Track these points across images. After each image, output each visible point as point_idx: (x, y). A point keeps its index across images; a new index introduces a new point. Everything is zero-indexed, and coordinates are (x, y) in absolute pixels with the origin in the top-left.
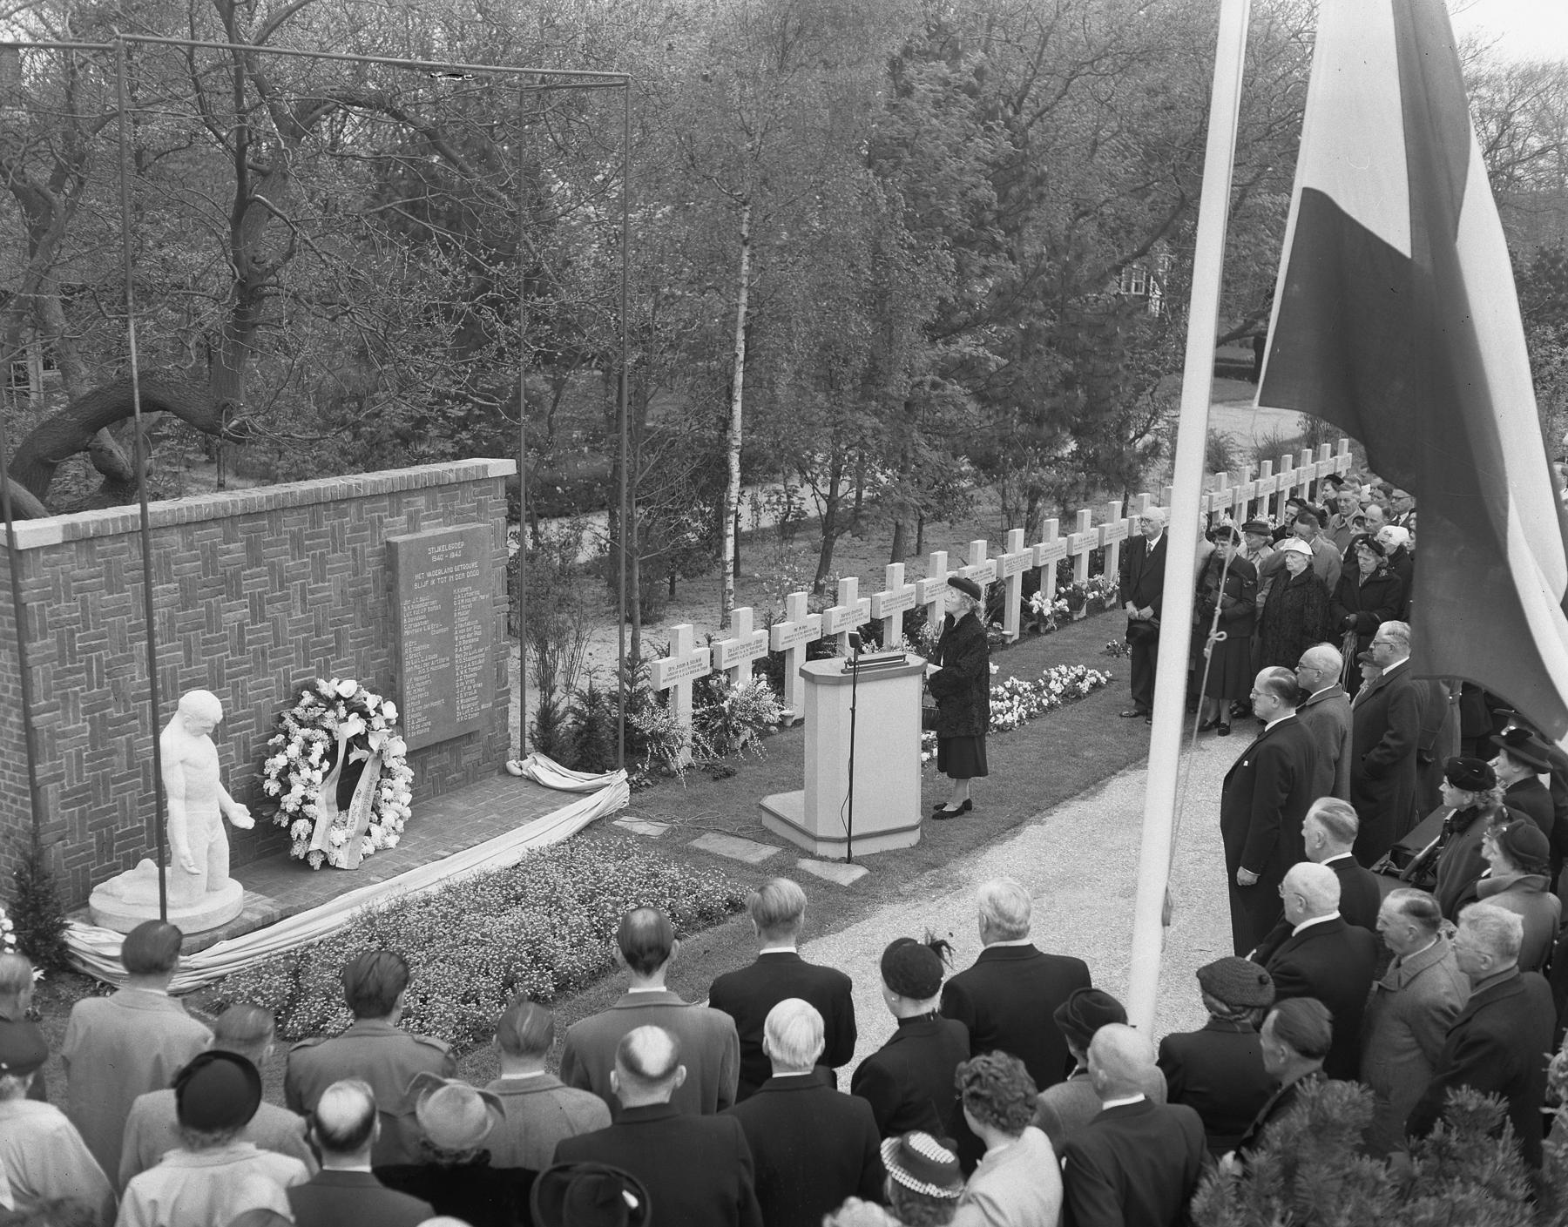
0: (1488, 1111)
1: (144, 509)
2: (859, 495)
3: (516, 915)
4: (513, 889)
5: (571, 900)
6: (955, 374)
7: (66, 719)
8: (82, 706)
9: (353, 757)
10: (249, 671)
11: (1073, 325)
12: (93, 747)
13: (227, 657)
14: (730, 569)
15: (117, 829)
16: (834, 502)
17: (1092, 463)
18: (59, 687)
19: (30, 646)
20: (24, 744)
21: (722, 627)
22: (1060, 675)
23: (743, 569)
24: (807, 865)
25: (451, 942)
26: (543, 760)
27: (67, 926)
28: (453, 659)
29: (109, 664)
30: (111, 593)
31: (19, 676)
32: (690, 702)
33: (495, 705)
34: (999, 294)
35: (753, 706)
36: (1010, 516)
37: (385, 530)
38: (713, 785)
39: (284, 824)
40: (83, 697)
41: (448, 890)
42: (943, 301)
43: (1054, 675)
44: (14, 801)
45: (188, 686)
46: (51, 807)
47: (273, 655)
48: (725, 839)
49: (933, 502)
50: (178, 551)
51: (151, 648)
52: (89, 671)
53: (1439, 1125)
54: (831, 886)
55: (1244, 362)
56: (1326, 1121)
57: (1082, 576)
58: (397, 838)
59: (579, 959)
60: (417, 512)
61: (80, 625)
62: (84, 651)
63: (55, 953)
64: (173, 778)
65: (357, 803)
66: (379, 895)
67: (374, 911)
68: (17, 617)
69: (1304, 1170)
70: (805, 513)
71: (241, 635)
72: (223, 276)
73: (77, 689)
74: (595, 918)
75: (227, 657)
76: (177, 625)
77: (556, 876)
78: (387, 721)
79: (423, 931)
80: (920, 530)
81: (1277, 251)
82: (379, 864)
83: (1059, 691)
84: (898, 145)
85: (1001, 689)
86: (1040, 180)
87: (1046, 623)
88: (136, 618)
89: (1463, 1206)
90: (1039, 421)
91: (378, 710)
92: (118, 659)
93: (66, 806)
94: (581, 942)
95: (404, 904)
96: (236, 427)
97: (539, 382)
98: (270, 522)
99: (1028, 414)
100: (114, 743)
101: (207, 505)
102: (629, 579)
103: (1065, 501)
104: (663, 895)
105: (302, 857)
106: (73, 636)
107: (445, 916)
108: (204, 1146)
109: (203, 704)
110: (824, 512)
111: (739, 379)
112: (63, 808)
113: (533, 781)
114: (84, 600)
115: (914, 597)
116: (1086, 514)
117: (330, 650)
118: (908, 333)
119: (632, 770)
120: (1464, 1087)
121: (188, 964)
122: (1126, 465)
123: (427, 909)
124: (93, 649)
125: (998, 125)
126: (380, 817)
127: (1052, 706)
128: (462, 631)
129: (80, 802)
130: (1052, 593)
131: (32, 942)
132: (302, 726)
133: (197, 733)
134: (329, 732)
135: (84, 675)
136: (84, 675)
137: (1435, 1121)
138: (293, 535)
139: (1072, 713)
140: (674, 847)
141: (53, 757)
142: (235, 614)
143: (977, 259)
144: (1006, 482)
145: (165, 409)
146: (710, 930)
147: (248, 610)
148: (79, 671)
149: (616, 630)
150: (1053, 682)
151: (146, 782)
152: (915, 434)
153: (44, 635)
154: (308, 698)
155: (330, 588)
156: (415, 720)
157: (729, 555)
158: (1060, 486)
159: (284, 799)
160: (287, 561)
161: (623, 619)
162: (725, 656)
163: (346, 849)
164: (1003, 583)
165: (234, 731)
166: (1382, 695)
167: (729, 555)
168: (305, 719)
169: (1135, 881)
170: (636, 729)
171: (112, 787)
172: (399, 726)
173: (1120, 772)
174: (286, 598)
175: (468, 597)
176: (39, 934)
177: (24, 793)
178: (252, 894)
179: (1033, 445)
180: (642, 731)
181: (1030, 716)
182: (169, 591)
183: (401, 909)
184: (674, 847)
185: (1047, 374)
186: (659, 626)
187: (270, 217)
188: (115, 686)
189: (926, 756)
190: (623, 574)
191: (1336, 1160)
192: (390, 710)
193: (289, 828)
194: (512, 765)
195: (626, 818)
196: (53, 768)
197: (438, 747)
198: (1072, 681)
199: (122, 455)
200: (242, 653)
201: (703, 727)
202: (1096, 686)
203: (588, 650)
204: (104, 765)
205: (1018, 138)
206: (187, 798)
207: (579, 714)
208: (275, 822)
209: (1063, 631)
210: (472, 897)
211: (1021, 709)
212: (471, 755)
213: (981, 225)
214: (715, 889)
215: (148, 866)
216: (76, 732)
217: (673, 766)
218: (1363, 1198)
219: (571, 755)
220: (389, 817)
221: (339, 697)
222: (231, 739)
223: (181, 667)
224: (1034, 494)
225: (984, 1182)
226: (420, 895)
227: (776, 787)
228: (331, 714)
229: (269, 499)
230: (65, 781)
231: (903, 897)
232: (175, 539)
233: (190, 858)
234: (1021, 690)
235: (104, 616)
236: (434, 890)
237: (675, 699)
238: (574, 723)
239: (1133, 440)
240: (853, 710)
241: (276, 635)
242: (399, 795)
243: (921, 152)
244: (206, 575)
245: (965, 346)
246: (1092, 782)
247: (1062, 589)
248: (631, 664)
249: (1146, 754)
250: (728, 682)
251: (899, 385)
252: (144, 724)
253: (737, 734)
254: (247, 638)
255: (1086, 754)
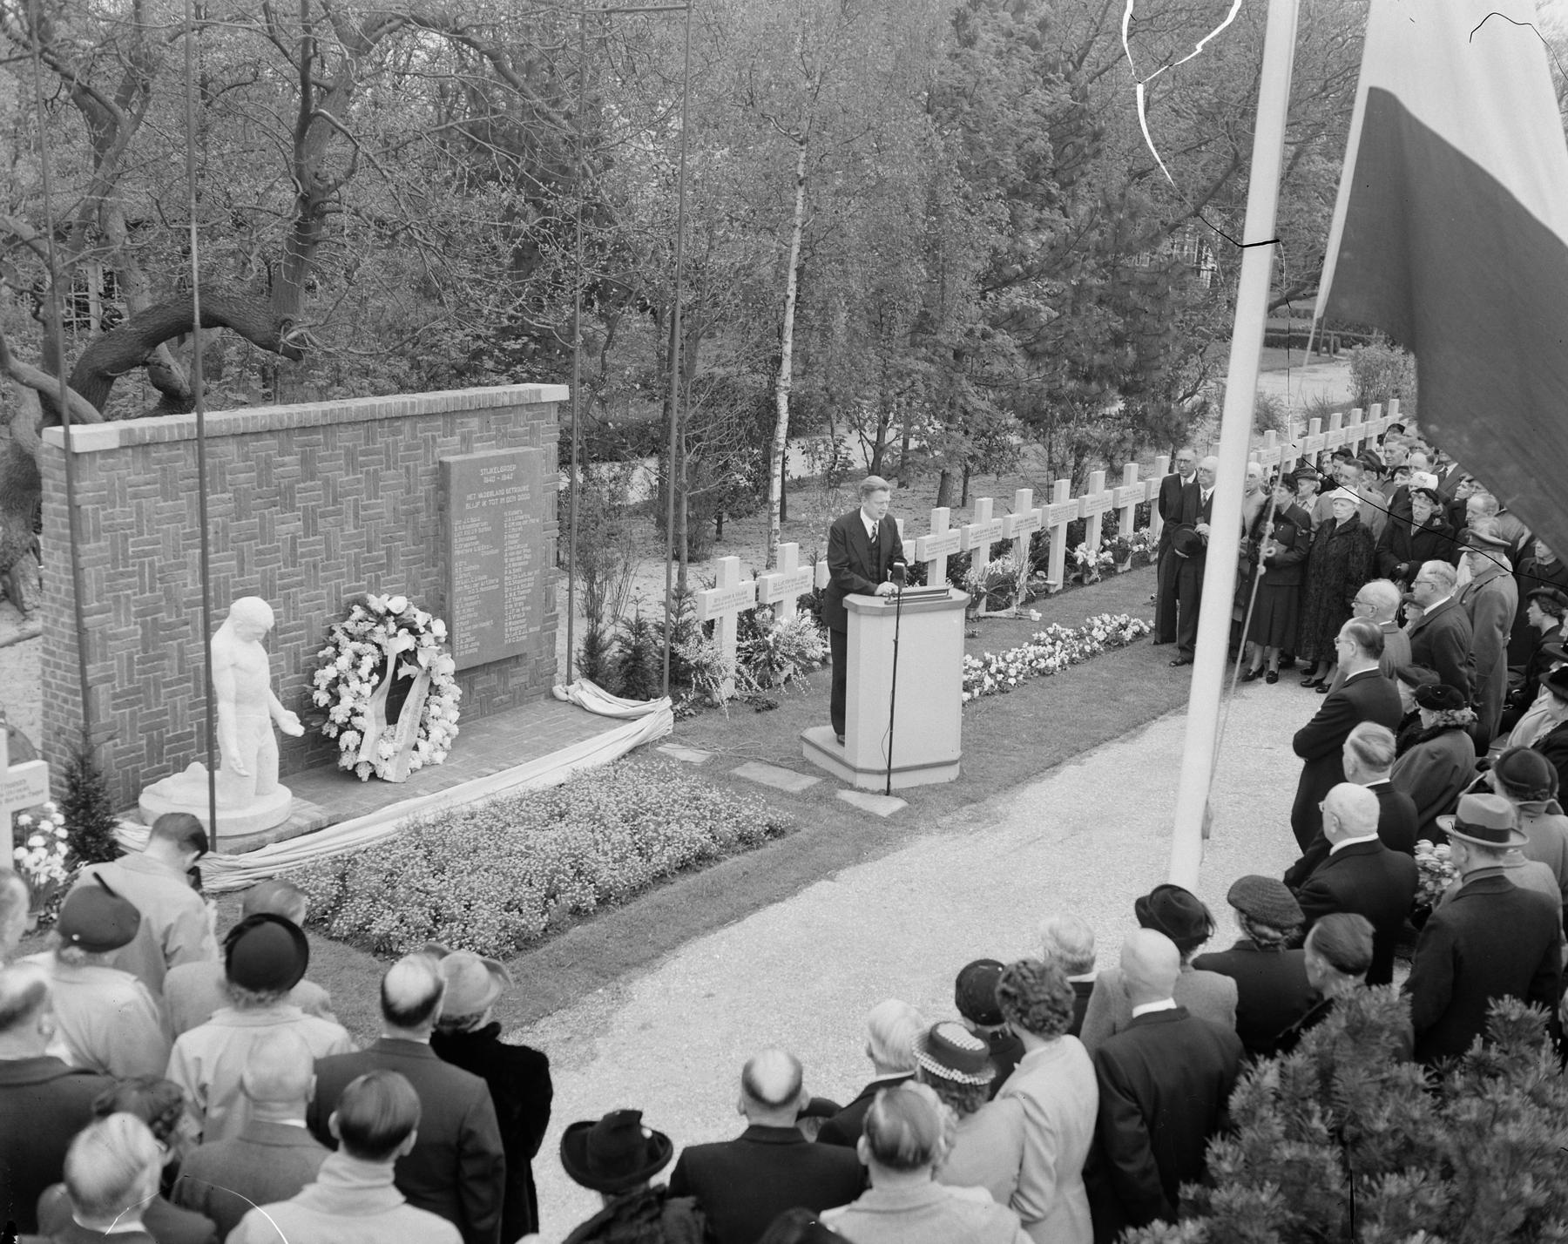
0: (1530, 1020)
1: (200, 418)
2: (906, 443)
3: (558, 830)
4: (557, 806)
5: (614, 819)
6: (1006, 324)
7: (118, 621)
8: (133, 609)
9: (402, 673)
10: (301, 584)
11: (1124, 283)
12: (145, 651)
13: (279, 568)
14: (777, 509)
15: (168, 732)
16: (882, 449)
17: (1140, 420)
18: (111, 589)
19: (82, 548)
20: (75, 644)
21: (768, 567)
22: (1103, 623)
23: (789, 514)
24: (846, 795)
25: (496, 853)
26: (589, 686)
27: (115, 825)
28: (502, 582)
29: (161, 570)
30: (166, 501)
31: (71, 577)
32: (735, 635)
33: (544, 629)
34: (1052, 248)
35: (796, 640)
36: (1056, 469)
37: (438, 450)
38: (755, 718)
39: (333, 734)
40: (136, 601)
41: (494, 805)
42: (996, 251)
43: (1097, 622)
44: (65, 701)
45: (238, 596)
46: (102, 707)
47: (325, 569)
48: (766, 768)
49: (980, 453)
50: (233, 460)
51: (204, 555)
52: (142, 576)
53: (1478, 1041)
54: (868, 817)
55: (1295, 331)
56: (1363, 1022)
57: (1127, 529)
58: (445, 755)
59: (621, 875)
60: (471, 432)
61: (134, 531)
62: (137, 555)
63: (105, 851)
64: (224, 682)
65: (405, 717)
66: (425, 807)
67: (421, 821)
68: (71, 519)
69: (1339, 1072)
70: (851, 463)
71: (294, 548)
72: (286, 195)
73: (129, 592)
74: (637, 837)
75: (279, 568)
76: (231, 535)
77: (601, 796)
78: (436, 638)
79: (468, 842)
80: (966, 483)
81: (1328, 218)
82: (425, 777)
83: (1102, 639)
84: (958, 94)
85: (1043, 635)
86: (1096, 136)
87: (1090, 574)
88: (191, 526)
89: (1506, 1107)
90: (1087, 378)
91: (428, 627)
92: (171, 565)
93: (117, 707)
94: (623, 858)
95: (450, 817)
96: (295, 339)
97: (591, 325)
98: (325, 437)
99: (1077, 370)
100: (165, 647)
101: (264, 417)
102: (678, 517)
103: (1112, 457)
104: (704, 817)
105: (350, 768)
106: (127, 540)
107: (490, 828)
108: (248, 1004)
109: (255, 611)
110: (871, 457)
111: (790, 320)
112: (114, 709)
113: (580, 707)
114: (139, 506)
115: (959, 543)
116: (1132, 469)
117: (381, 567)
118: (963, 283)
119: (676, 699)
120: (1507, 996)
121: (236, 864)
122: (1174, 423)
123: (473, 821)
124: (147, 554)
125: (1058, 78)
126: (427, 732)
127: (1094, 653)
128: (512, 554)
129: (131, 704)
130: (1097, 545)
131: (82, 839)
132: (352, 639)
133: (248, 639)
134: (379, 647)
135: (136, 579)
136: (136, 579)
137: (1474, 1037)
138: (347, 449)
139: (1114, 659)
140: (715, 772)
141: (104, 658)
142: (288, 526)
143: (1030, 213)
144: (1053, 436)
145: (225, 325)
146: (749, 853)
147: (300, 523)
148: (131, 575)
149: (663, 567)
150: (1096, 630)
151: (197, 689)
152: (964, 382)
153: (97, 538)
154: (358, 612)
155: (383, 505)
156: (464, 639)
157: (776, 495)
158: (1107, 443)
159: (333, 710)
160: (341, 476)
161: (671, 557)
162: (770, 590)
163: (394, 763)
164: (1047, 534)
165: (285, 641)
166: (1422, 636)
167: (776, 495)
168: (355, 633)
169: (1172, 821)
170: (681, 659)
171: (163, 691)
172: (448, 643)
173: (1161, 717)
174: (338, 513)
175: (518, 520)
176: (89, 831)
177: (75, 692)
178: (300, 800)
179: (1081, 401)
180: (686, 661)
181: (1072, 661)
182: (223, 501)
183: (447, 821)
184: (715, 772)
185: (1097, 329)
186: (705, 564)
187: (333, 133)
188: (167, 591)
189: (967, 696)
190: (671, 512)
191: (1373, 1064)
192: (439, 628)
193: (337, 739)
194: (559, 690)
195: (668, 745)
196: (104, 669)
197: (486, 667)
198: (1116, 630)
199: (180, 374)
200: (294, 566)
201: (747, 661)
202: (1139, 635)
203: (635, 584)
204: (155, 669)
205: (1077, 93)
206: (237, 702)
207: (627, 644)
208: (324, 733)
209: (1106, 582)
210: (517, 811)
211: (1063, 654)
212: (519, 678)
213: (1036, 178)
214: (756, 815)
215: (198, 769)
216: (126, 635)
217: (716, 698)
218: (1402, 1102)
219: (618, 683)
220: (436, 733)
221: (389, 613)
222: (281, 649)
223: (234, 576)
224: (1080, 450)
225: (1022, 1080)
226: (466, 809)
227: (818, 721)
228: (380, 629)
229: (325, 414)
230: (116, 682)
231: (943, 830)
232: (230, 449)
233: (239, 760)
234: (1063, 636)
235: (159, 522)
236: (480, 805)
237: (721, 630)
238: (621, 651)
239: (1182, 399)
240: (896, 643)
241: (328, 548)
242: (447, 711)
243: (980, 102)
244: (260, 486)
245: (1016, 297)
246: (1134, 725)
247: (1107, 542)
248: (679, 595)
249: (1186, 701)
250: (772, 618)
251: (951, 334)
252: (195, 629)
253: (781, 669)
254: (300, 550)
255: (1127, 698)
